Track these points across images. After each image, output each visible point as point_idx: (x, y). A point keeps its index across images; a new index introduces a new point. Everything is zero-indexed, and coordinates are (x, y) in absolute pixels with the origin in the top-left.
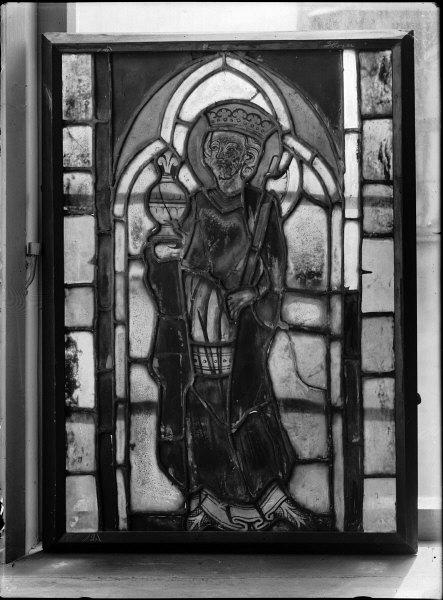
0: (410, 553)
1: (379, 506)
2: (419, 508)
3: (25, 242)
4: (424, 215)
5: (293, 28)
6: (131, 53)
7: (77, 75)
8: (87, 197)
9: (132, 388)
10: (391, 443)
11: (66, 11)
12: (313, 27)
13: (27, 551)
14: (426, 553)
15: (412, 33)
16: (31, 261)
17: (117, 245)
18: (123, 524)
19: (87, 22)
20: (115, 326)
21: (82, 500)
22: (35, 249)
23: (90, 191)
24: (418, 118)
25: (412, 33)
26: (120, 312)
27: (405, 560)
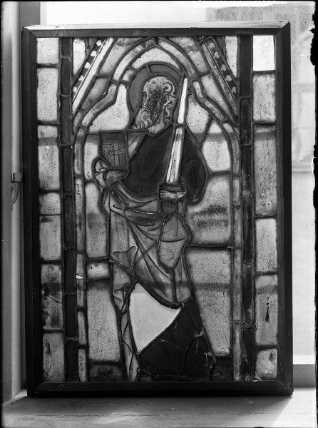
0: (287, 394)
1: (267, 365)
2: (294, 363)
3: (11, 171)
4: (298, 152)
5: (204, 19)
6: (86, 241)
7: (47, 50)
8: (57, 284)
9: (87, 205)
10: (297, 129)
11: (39, 9)
12: (217, 18)
13: (13, 396)
14: (301, 399)
15: (288, 25)
16: (15, 186)
17: (76, 155)
18: (83, 375)
19: (54, 16)
20: (75, 178)
21: (54, 362)
22: (18, 178)
23: (59, 280)
24: (293, 83)
25: (288, 25)
26: (80, 302)
27: (280, 401)
